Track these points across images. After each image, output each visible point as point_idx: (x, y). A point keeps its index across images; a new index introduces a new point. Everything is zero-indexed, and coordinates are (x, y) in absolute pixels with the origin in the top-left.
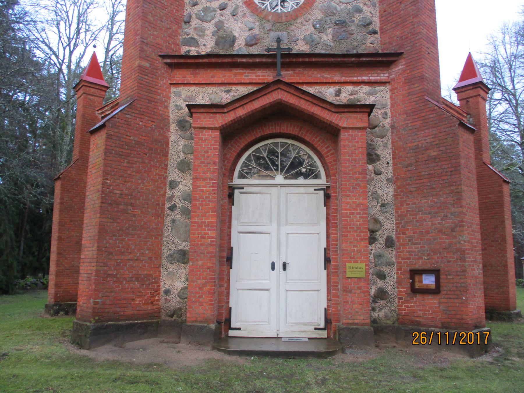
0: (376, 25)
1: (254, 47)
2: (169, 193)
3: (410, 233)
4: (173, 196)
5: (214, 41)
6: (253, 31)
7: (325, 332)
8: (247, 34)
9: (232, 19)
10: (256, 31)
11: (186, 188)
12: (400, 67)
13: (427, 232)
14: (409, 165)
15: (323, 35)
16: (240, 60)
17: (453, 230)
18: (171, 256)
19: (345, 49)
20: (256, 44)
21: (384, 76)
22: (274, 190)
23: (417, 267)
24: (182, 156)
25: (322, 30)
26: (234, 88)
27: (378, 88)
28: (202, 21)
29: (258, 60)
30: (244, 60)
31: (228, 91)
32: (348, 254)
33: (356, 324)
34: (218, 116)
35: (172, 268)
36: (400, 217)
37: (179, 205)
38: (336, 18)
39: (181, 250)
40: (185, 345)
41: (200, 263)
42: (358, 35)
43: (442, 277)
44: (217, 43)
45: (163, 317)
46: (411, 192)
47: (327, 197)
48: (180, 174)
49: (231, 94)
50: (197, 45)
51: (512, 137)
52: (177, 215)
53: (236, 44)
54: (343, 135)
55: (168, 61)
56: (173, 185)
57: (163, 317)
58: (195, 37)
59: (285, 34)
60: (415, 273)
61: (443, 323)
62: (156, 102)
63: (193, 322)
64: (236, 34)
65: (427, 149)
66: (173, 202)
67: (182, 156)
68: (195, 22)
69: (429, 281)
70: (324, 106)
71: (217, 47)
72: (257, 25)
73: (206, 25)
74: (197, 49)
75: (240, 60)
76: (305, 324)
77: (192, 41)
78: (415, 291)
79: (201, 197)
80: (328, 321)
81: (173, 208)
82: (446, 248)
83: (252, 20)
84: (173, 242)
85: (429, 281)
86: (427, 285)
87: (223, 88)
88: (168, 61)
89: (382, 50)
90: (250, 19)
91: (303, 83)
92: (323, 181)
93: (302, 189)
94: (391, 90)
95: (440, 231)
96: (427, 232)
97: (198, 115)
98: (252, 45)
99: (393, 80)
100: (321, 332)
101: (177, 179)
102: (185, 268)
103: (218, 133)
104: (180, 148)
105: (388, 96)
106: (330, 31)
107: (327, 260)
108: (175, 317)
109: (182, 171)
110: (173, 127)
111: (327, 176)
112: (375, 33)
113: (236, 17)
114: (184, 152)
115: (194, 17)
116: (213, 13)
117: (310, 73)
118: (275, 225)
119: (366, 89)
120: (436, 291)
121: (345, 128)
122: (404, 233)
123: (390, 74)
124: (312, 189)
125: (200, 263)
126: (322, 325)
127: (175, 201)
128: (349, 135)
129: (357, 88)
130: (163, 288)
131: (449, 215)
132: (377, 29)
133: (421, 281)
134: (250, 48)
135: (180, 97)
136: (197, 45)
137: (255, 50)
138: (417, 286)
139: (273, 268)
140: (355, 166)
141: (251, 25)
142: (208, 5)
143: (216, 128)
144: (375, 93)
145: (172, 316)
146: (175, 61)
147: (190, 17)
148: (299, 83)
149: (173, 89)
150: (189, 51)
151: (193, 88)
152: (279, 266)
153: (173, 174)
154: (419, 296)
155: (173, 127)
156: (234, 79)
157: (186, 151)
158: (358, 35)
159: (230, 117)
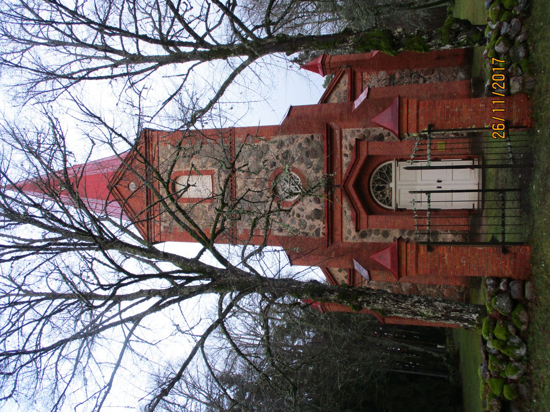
0: (308, 136)
5: (317, 220)
8: (313, 203)
21: (337, 132)
22: (398, 188)
24: (380, 235)
27: (343, 135)
38: (304, 156)
44: (318, 219)
48: (390, 236)
58: (315, 230)
64: (313, 209)
67: (380, 235)
68: (307, 230)
73: (308, 224)
77: (318, 231)
92: (393, 162)
93: (398, 173)
101: (392, 238)
105: (348, 129)
106: (311, 160)
112: (312, 137)
114: (378, 234)
124: (398, 168)
132: (310, 135)
141: (308, 201)
143: (368, 217)
146: (330, 239)
155: (365, 240)
158: (314, 145)
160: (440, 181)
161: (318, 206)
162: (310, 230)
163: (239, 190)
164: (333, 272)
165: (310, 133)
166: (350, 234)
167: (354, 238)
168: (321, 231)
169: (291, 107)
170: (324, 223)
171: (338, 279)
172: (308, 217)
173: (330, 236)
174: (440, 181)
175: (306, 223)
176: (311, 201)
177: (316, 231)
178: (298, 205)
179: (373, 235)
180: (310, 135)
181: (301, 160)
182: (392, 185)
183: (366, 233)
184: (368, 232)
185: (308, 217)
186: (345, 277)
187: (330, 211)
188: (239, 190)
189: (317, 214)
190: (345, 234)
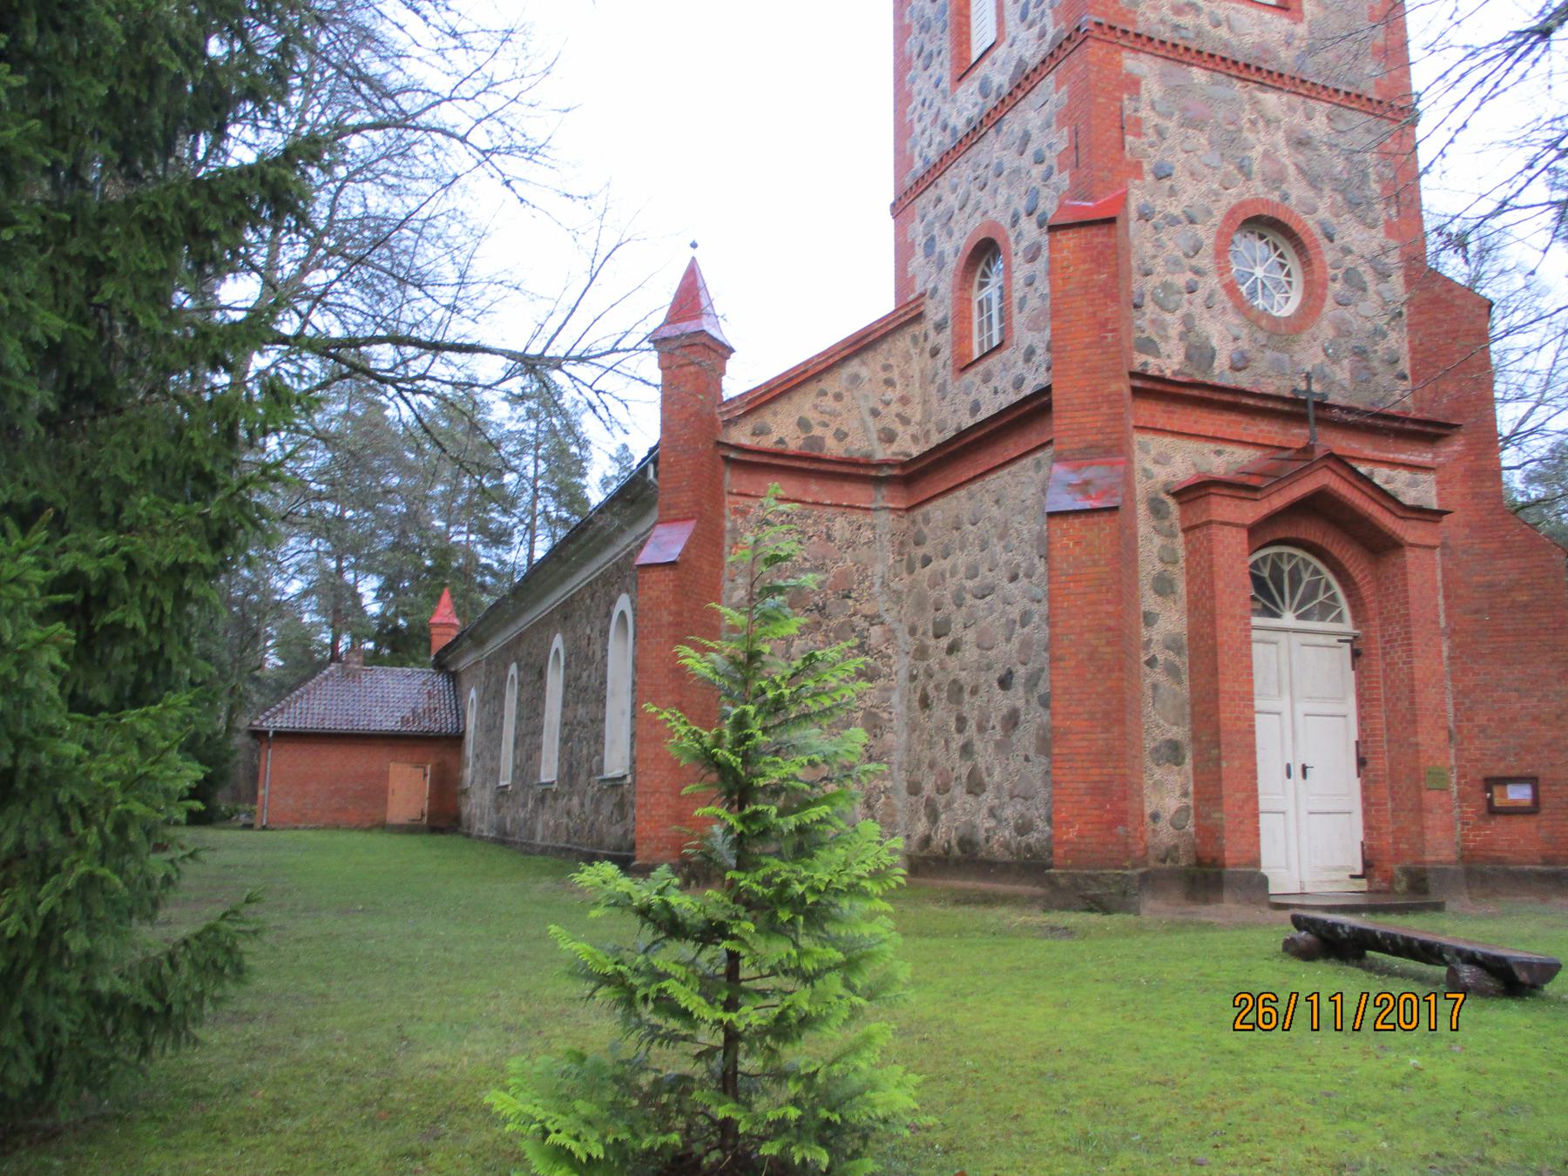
0: (1405, 365)
1: (1243, 373)
2: (1145, 633)
3: (1481, 719)
4: (1150, 641)
5: (1182, 352)
7: (1364, 881)
8: (1231, 346)
10: (1244, 344)
11: (1170, 627)
12: (1454, 447)
13: (1513, 720)
14: (1476, 612)
15: (1336, 368)
16: (1246, 400)
17: (1558, 717)
18: (1156, 750)
21: (1425, 457)
22: (1282, 636)
23: (1496, 773)
24: (1159, 566)
25: (1335, 360)
26: (1229, 448)
27: (1421, 476)
28: (1163, 308)
29: (1270, 405)
30: (1251, 402)
31: (1218, 453)
33: (1440, 862)
34: (1246, 505)
35: (1158, 773)
36: (1461, 694)
37: (1161, 658)
38: (1354, 342)
39: (1170, 741)
40: (1232, 906)
41: (1237, 763)
42: (1385, 379)
43: (1542, 788)
44: (1188, 357)
45: (1152, 863)
46: (1483, 656)
47: (1356, 654)
48: (1159, 599)
49: (1224, 458)
50: (1157, 354)
51: (423, 377)
52: (1158, 676)
53: (1216, 364)
55: (1138, 383)
56: (1150, 619)
57: (1152, 863)
58: (1156, 339)
59: (1286, 357)
60: (1491, 783)
61: (1543, 857)
63: (1235, 865)
64: (1215, 342)
65: (1509, 590)
67: (1159, 566)
68: (1150, 309)
69: (1519, 794)
70: (1387, 504)
72: (1244, 333)
73: (1168, 317)
75: (1246, 400)
76: (1336, 870)
77: (1149, 346)
78: (1493, 811)
79: (1231, 648)
80: (1367, 864)
81: (1151, 662)
82: (1548, 745)
83: (1237, 322)
84: (1158, 726)
85: (1519, 794)
86: (1515, 801)
87: (1212, 446)
88: (1138, 383)
89: (1421, 410)
90: (1233, 319)
91: (1354, 458)
92: (1347, 626)
93: (1320, 639)
94: (1438, 483)
95: (1535, 719)
96: (1513, 720)
97: (1218, 499)
98: (1239, 370)
99: (1443, 465)
100: (1358, 881)
101: (1156, 609)
103: (1244, 535)
104: (1155, 550)
105: (1434, 492)
106: (1345, 362)
107: (1361, 763)
108: (1169, 864)
110: (1142, 510)
111: (1355, 617)
112: (1404, 377)
114: (1162, 560)
115: (1148, 298)
116: (1177, 297)
118: (1287, 698)
119: (1403, 475)
120: (1532, 810)
121: (1412, 545)
122: (1469, 720)
123: (1436, 456)
124: (1333, 640)
125: (1237, 763)
126: (1359, 870)
127: (1156, 650)
129: (1394, 473)
130: (1148, 811)
131: (1552, 696)
132: (1407, 372)
133: (1504, 795)
135: (1147, 452)
136: (1157, 354)
138: (1497, 802)
139: (1289, 775)
141: (1235, 331)
142: (1169, 278)
143: (1243, 526)
144: (1413, 484)
145: (1164, 861)
146: (1149, 385)
147: (1142, 296)
148: (1354, 458)
149: (1138, 437)
150: (1145, 364)
151: (1168, 440)
152: (1297, 771)
153: (1149, 601)
154: (1500, 819)
155: (1142, 510)
156: (1227, 432)
158: (1385, 379)
160: (1304, 775)
161: (1222, 362)
162: (1153, 322)
163: (1251, 98)
164: (797, 397)
165: (1414, 372)
166: (1156, 462)
167: (1148, 474)
168: (1151, 360)
169: (731, 350)
170: (1174, 373)
171: (775, 414)
172: (1188, 321)
173: (1159, 387)
174: (1304, 775)
175: (1172, 311)
176: (1236, 339)
177: (1149, 340)
178: (1222, 295)
179: (1158, 541)
180: (1407, 372)
181: (1343, 330)
182: (1289, 619)
183: (1163, 518)
184: (1167, 523)
185: (1188, 321)
186: (781, 441)
187: (1227, 398)
188: (1251, 98)
189: (1200, 353)
190: (1158, 443)
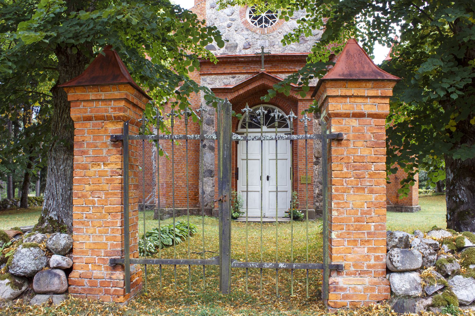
1: (249, 50)
6: (248, 40)
9: (235, 33)
19: (303, 50)
20: (250, 48)
31: (234, 77)
32: (302, 171)
37: (207, 145)
48: (208, 126)
54: (300, 104)
62: (303, 305)
66: (204, 143)
71: (226, 50)
74: (215, 52)
87: (231, 76)
102: (212, 180)
109: (208, 125)
113: (237, 32)
117: (282, 66)
128: (303, 104)
134: (247, 50)
137: (249, 52)
140: (99, 176)
157: (210, 113)
159: (236, 94)
